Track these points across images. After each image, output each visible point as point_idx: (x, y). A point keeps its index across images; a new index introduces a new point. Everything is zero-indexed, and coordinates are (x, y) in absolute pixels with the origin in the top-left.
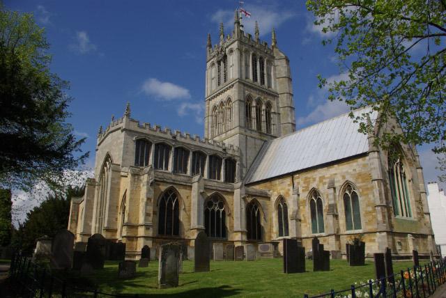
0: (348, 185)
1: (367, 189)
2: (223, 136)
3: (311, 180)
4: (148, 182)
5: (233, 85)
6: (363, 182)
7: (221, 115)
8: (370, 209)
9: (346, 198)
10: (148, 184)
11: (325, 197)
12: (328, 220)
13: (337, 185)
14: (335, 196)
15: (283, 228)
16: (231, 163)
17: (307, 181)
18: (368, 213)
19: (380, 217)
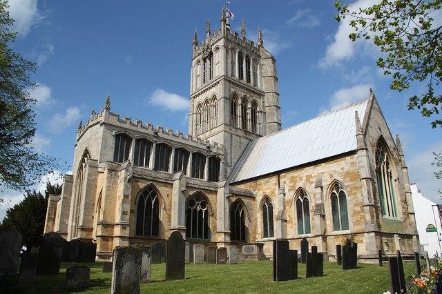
0: (336, 185)
1: (356, 188)
2: (208, 134)
3: (298, 179)
4: (125, 178)
5: (218, 83)
6: (351, 180)
7: (206, 113)
8: (358, 209)
9: (333, 197)
10: (125, 181)
11: (312, 196)
12: (315, 220)
13: (324, 184)
14: (322, 196)
15: (268, 229)
16: (215, 161)
17: (293, 180)
18: (356, 213)
19: (368, 217)
